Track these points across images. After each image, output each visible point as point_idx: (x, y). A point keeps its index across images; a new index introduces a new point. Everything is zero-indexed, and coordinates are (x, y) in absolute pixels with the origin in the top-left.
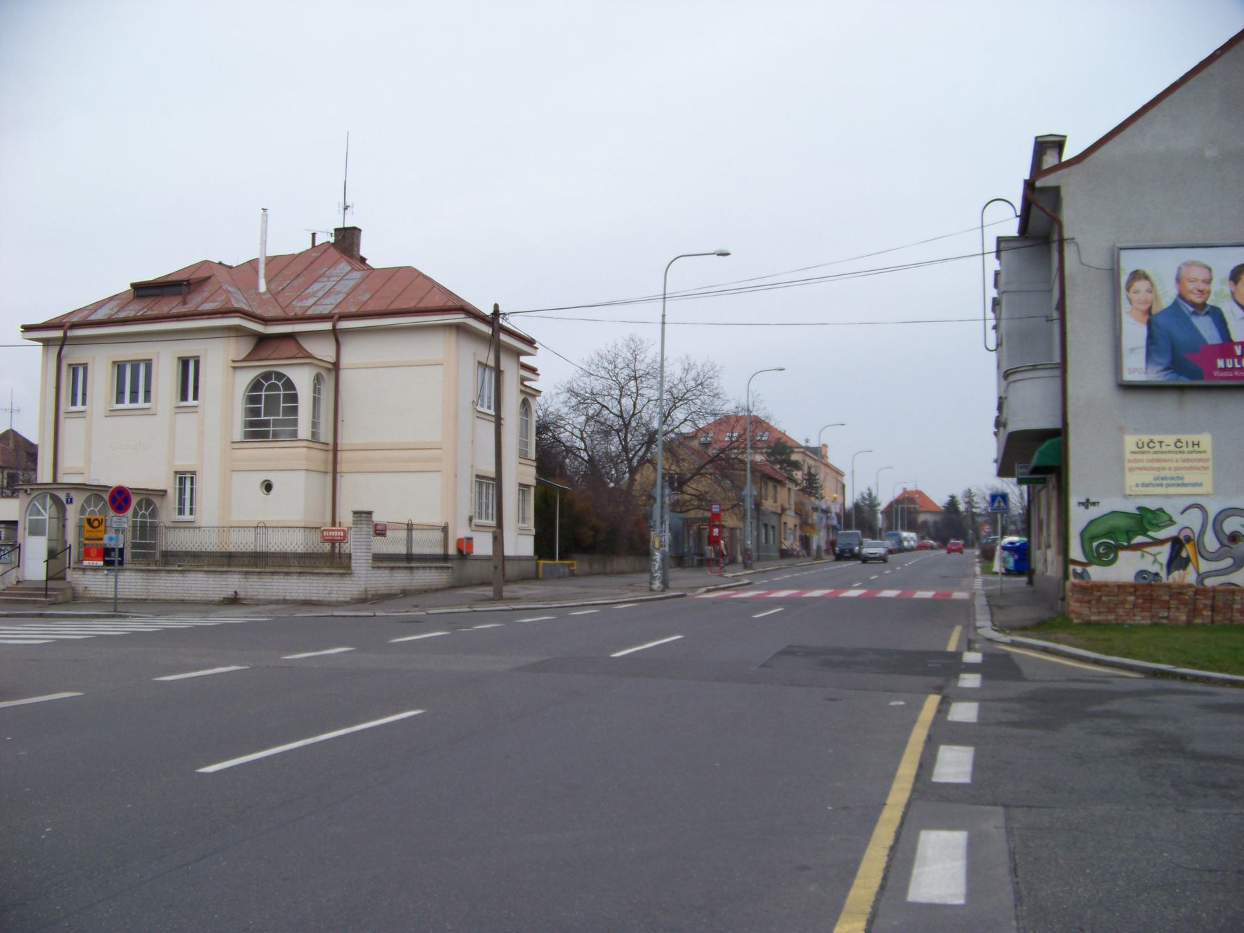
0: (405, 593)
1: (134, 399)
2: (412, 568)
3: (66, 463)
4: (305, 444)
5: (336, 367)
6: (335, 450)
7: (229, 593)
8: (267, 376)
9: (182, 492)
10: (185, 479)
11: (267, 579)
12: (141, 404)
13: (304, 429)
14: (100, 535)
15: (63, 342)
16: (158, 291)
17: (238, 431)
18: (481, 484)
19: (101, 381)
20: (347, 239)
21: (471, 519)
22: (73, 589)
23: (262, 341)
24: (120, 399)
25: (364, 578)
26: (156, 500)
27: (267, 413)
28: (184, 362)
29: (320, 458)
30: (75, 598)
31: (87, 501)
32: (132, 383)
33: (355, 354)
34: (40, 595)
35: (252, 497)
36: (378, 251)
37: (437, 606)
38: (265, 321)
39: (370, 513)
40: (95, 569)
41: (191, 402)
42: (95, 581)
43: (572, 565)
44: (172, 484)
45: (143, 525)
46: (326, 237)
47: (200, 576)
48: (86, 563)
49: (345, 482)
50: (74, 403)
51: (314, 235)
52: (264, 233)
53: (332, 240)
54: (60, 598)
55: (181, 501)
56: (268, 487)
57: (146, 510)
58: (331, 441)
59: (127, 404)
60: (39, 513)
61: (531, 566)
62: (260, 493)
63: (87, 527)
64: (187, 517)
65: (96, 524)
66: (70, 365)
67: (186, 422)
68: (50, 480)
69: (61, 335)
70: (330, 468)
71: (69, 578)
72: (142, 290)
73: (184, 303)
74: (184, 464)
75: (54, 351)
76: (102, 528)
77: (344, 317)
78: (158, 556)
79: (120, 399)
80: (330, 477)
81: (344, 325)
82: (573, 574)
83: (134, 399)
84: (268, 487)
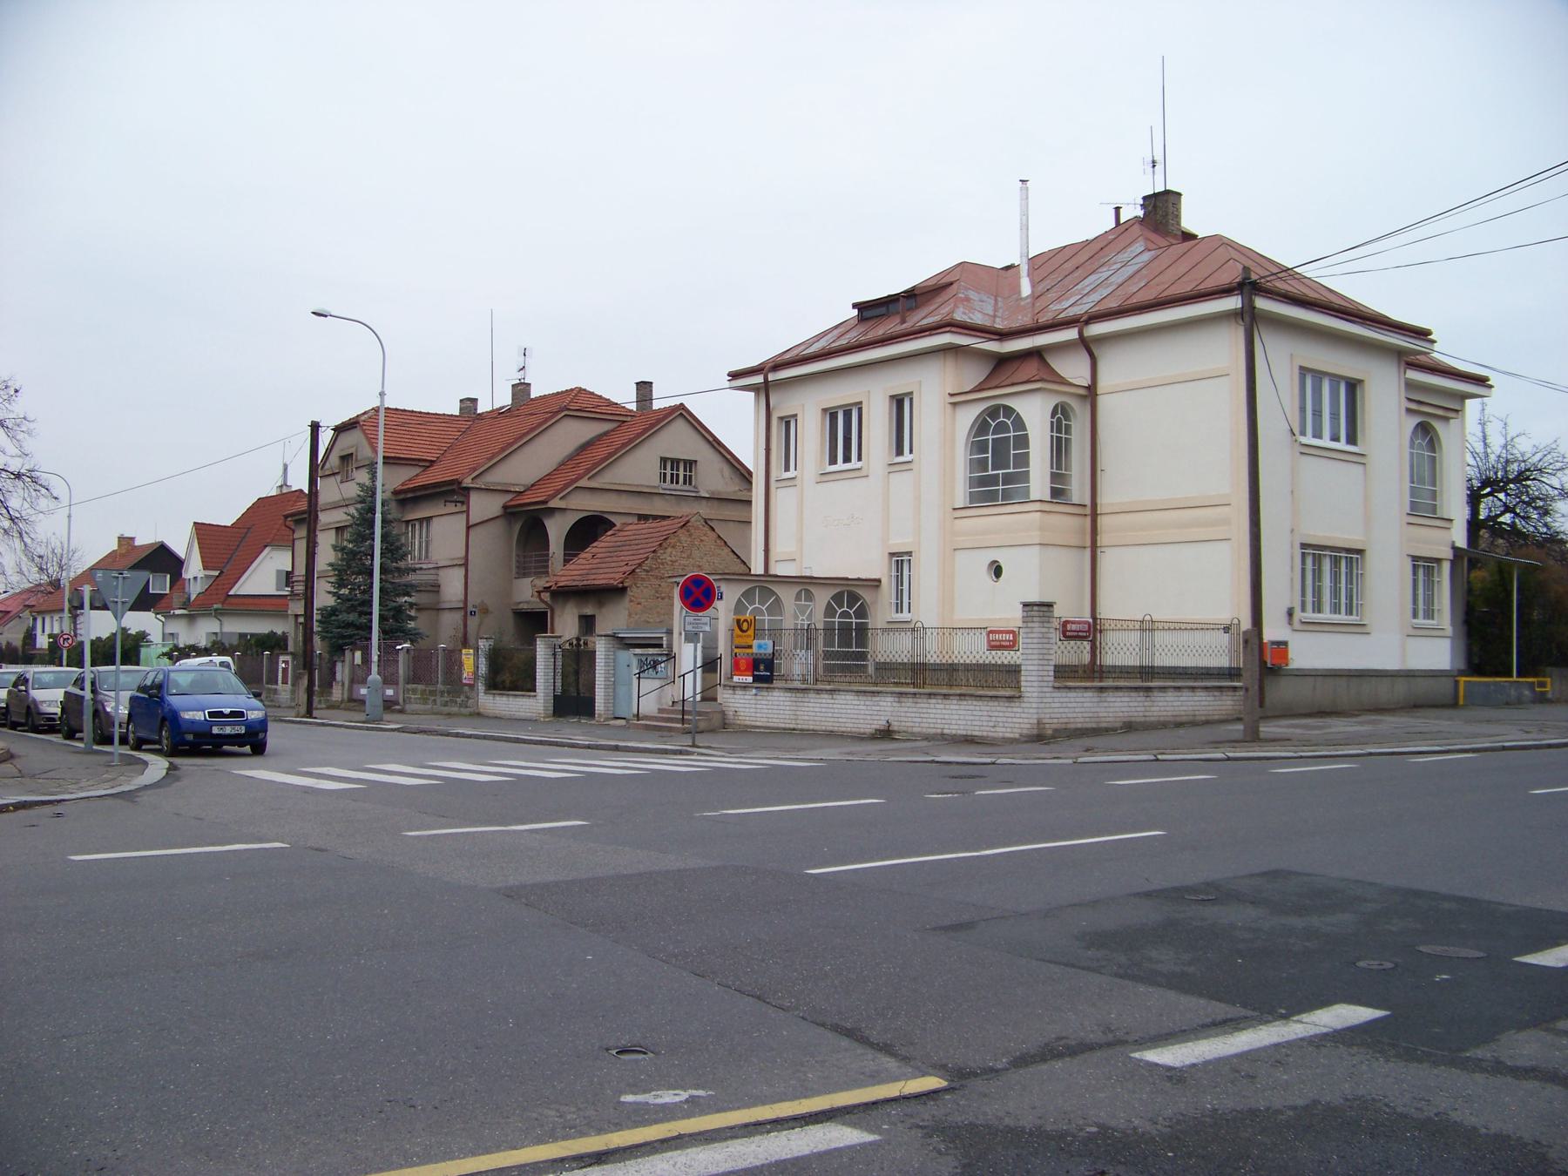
0: (1130, 727)
1: (847, 459)
2: (1149, 689)
3: (778, 549)
4: (1037, 506)
5: (1091, 393)
6: (1094, 516)
7: (880, 723)
9: (899, 580)
10: (900, 560)
11: (923, 704)
12: (854, 464)
13: (1039, 481)
14: (749, 641)
16: (883, 310)
17: (961, 495)
18: (1317, 560)
19: (811, 435)
20: (1161, 209)
21: (1290, 613)
22: (723, 713)
23: (1002, 362)
24: (833, 461)
25: (1041, 702)
26: (866, 595)
27: (995, 468)
29: (1068, 525)
30: (723, 725)
31: (748, 595)
33: (1116, 370)
35: (971, 582)
36: (1192, 219)
37: (1174, 749)
38: (1003, 335)
39: (1050, 605)
40: (745, 687)
41: (907, 457)
42: (747, 704)
43: (1542, 685)
44: (886, 570)
45: (845, 629)
46: (1132, 211)
48: (736, 679)
51: (1117, 209)
52: (1025, 214)
53: (1141, 213)
54: (702, 725)
55: (899, 593)
56: (997, 571)
57: (850, 607)
58: (1088, 502)
59: (840, 466)
61: (1445, 686)
62: (986, 578)
63: (737, 631)
64: (905, 616)
65: (745, 626)
66: (781, 418)
67: (901, 481)
68: (761, 572)
69: (765, 380)
72: (869, 311)
73: (903, 321)
74: (899, 543)
76: (751, 632)
78: (871, 670)
79: (833, 461)
80: (1088, 553)
81: (1096, 329)
82: (1542, 699)
83: (847, 459)
84: (997, 571)
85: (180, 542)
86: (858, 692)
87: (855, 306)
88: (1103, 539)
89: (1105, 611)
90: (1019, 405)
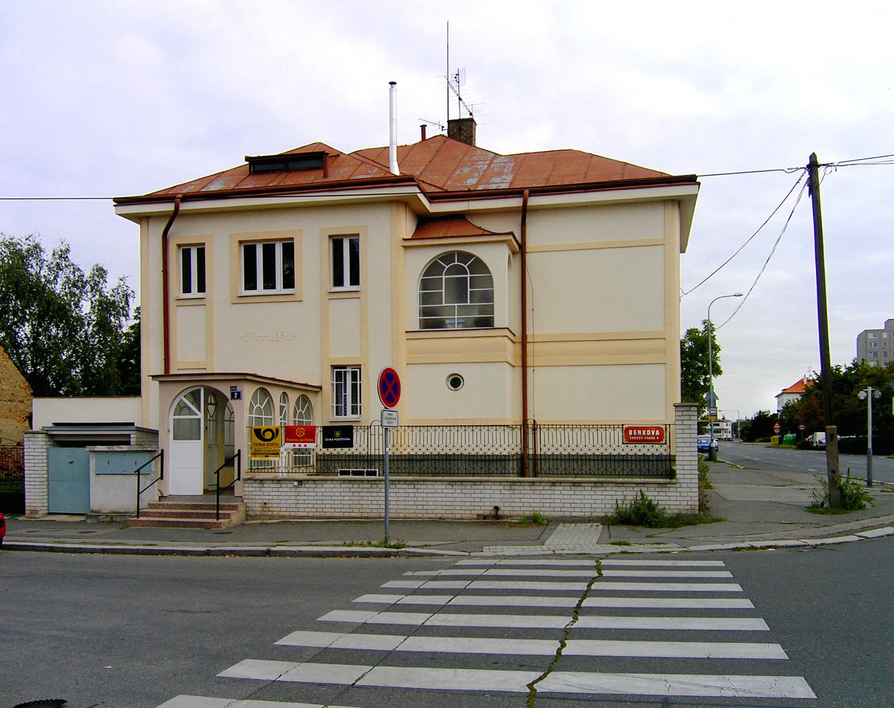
1: (270, 282)
7: (488, 509)
8: (447, 258)
15: (173, 217)
16: (281, 166)
17: (413, 320)
20: (462, 130)
28: (337, 243)
32: (266, 267)
34: (209, 516)
47: (440, 487)
49: (537, 378)
50: (187, 289)
51: (423, 127)
56: (456, 382)
60: (191, 412)
62: (445, 385)
64: (350, 416)
66: (179, 246)
69: (163, 211)
70: (520, 363)
71: (238, 492)
75: (158, 229)
77: (536, 192)
80: (519, 371)
81: (534, 201)
83: (270, 282)
84: (456, 382)
85: (424, 258)
86: (450, 482)
87: (247, 159)
88: (529, 362)
89: (537, 413)
90: (482, 253)
